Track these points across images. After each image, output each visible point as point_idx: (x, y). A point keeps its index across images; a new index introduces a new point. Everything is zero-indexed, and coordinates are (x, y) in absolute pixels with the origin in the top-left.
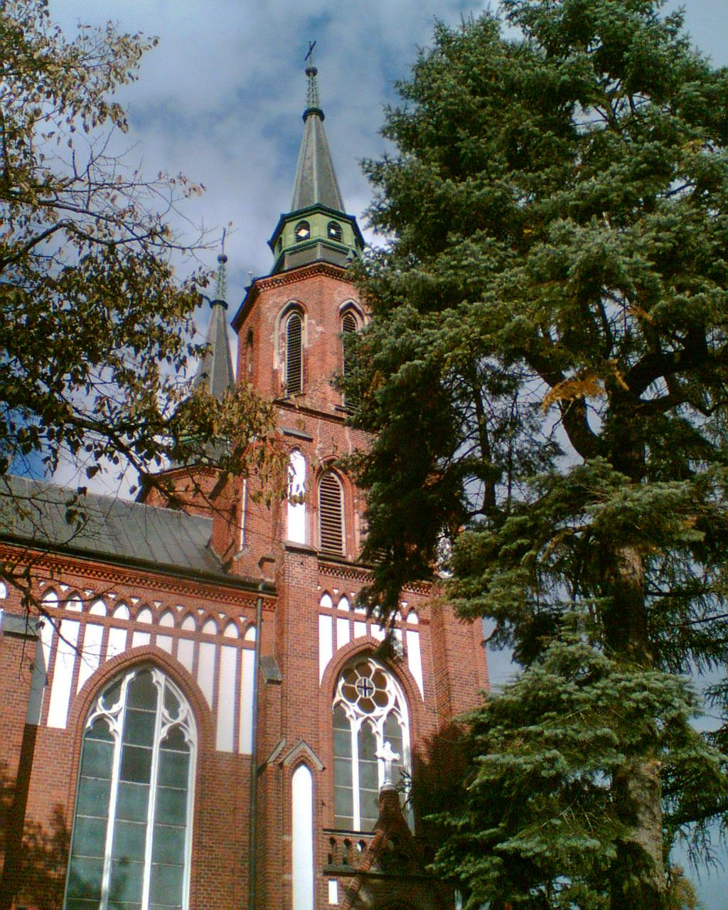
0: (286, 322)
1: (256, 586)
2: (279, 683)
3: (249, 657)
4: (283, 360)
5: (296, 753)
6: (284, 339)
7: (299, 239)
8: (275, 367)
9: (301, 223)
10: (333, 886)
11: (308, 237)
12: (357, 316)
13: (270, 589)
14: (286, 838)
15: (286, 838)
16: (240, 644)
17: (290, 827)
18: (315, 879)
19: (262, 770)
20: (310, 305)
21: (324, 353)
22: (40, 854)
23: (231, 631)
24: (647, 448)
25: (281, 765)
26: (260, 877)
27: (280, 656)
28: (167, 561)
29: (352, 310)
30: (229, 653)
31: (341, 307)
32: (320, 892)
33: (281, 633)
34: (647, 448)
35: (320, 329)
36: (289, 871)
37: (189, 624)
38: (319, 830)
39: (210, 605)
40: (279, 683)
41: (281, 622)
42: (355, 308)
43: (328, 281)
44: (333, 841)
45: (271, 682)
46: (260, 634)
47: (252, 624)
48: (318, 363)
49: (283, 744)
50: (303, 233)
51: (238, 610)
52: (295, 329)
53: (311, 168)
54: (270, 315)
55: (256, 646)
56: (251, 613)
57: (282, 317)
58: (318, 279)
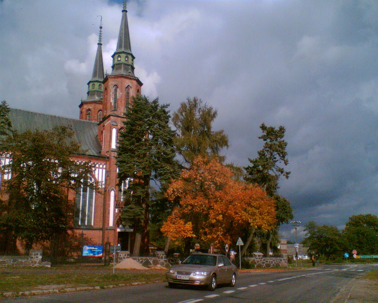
0: (114, 88)
1: (105, 158)
2: (109, 176)
3: (104, 170)
4: (113, 99)
5: (112, 189)
6: (113, 93)
7: (118, 60)
8: (111, 102)
9: (119, 55)
10: (117, 210)
11: (120, 60)
12: (130, 88)
13: (108, 158)
14: (109, 202)
15: (109, 202)
16: (103, 168)
17: (110, 200)
18: (114, 209)
19: (105, 191)
20: (119, 86)
21: (122, 100)
22: (72, 205)
23: (101, 166)
24: (47, 210)
25: (109, 191)
26: (105, 208)
27: (110, 171)
28: (93, 155)
29: (129, 87)
30: (101, 170)
31: (126, 86)
32: (114, 210)
33: (110, 167)
34: (47, 210)
35: (121, 93)
36: (110, 208)
37: (101, 166)
38: (115, 200)
39: (97, 161)
40: (109, 176)
41: (110, 165)
42: (130, 86)
43: (123, 79)
44: (117, 202)
45: (108, 176)
46: (106, 166)
47: (105, 165)
48: (120, 103)
49: (109, 187)
50: (119, 59)
51: (102, 162)
52: (116, 90)
53: (122, 34)
54: (110, 87)
55: (106, 169)
56: (104, 162)
57: (114, 87)
58: (121, 79)
